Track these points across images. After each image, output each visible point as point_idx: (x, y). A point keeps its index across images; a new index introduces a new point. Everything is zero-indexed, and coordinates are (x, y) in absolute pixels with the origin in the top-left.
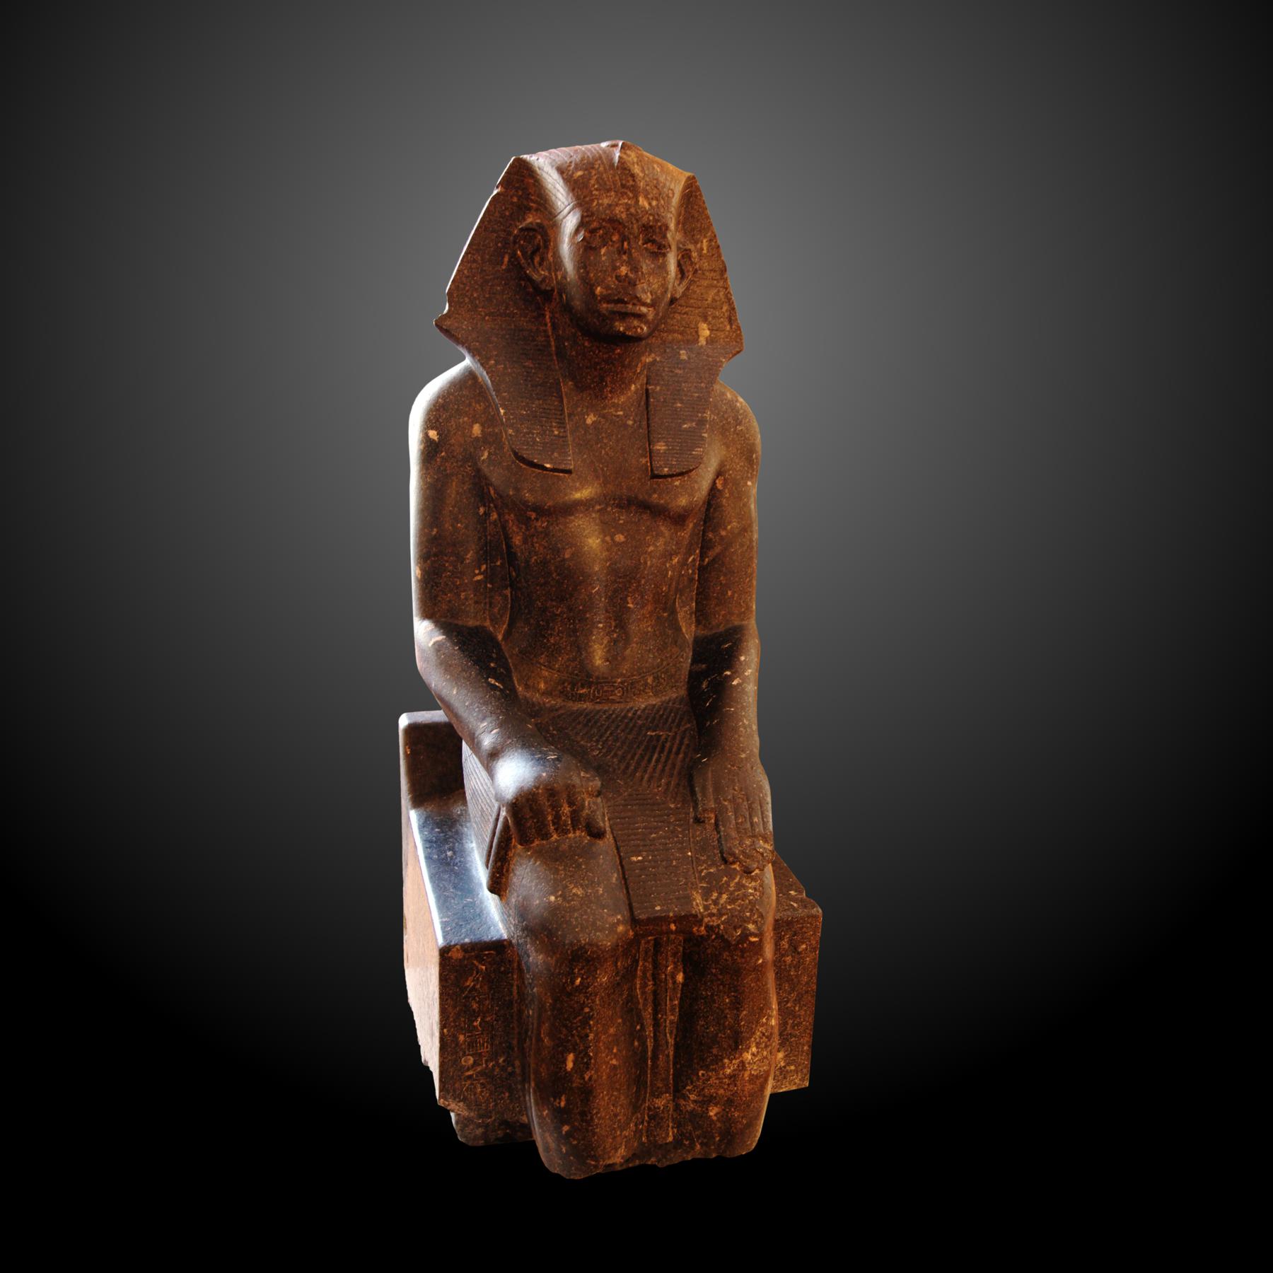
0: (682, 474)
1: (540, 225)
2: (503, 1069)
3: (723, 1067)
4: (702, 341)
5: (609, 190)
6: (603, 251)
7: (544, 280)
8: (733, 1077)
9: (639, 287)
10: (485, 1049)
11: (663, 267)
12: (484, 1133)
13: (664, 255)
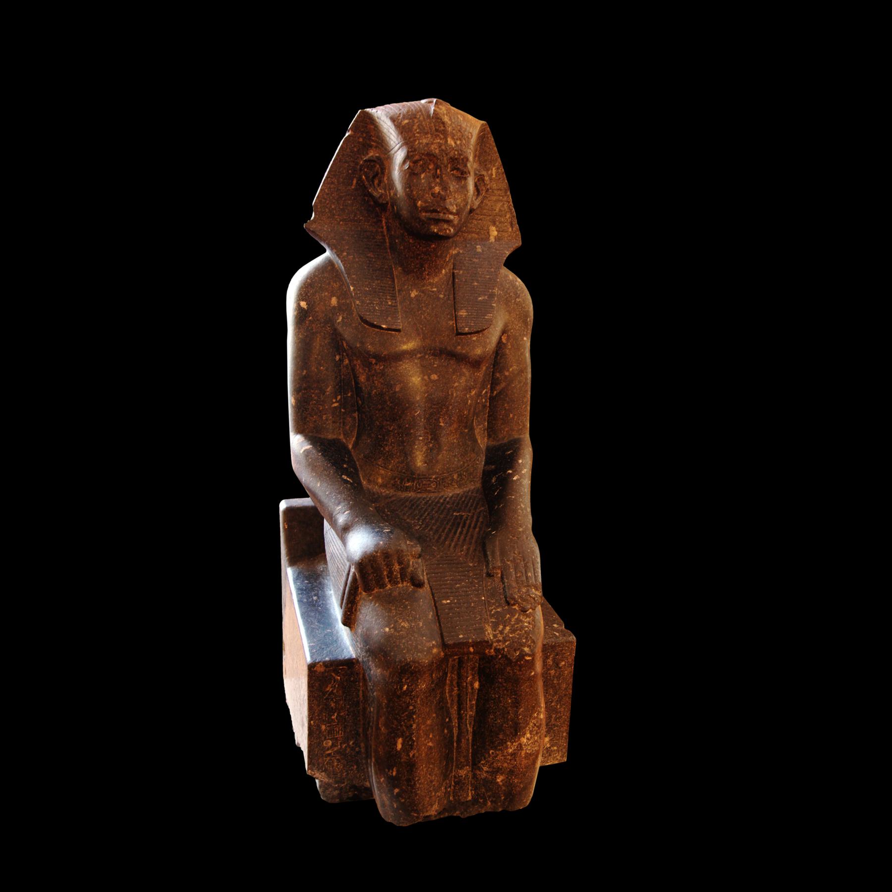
0: (478, 332)
1: (378, 158)
2: (353, 749)
3: (507, 748)
4: (492, 239)
5: (427, 133)
6: (423, 176)
7: (381, 196)
8: (513, 755)
9: (448, 201)
10: (340, 735)
11: (465, 187)
12: (339, 794)
13: (465, 179)
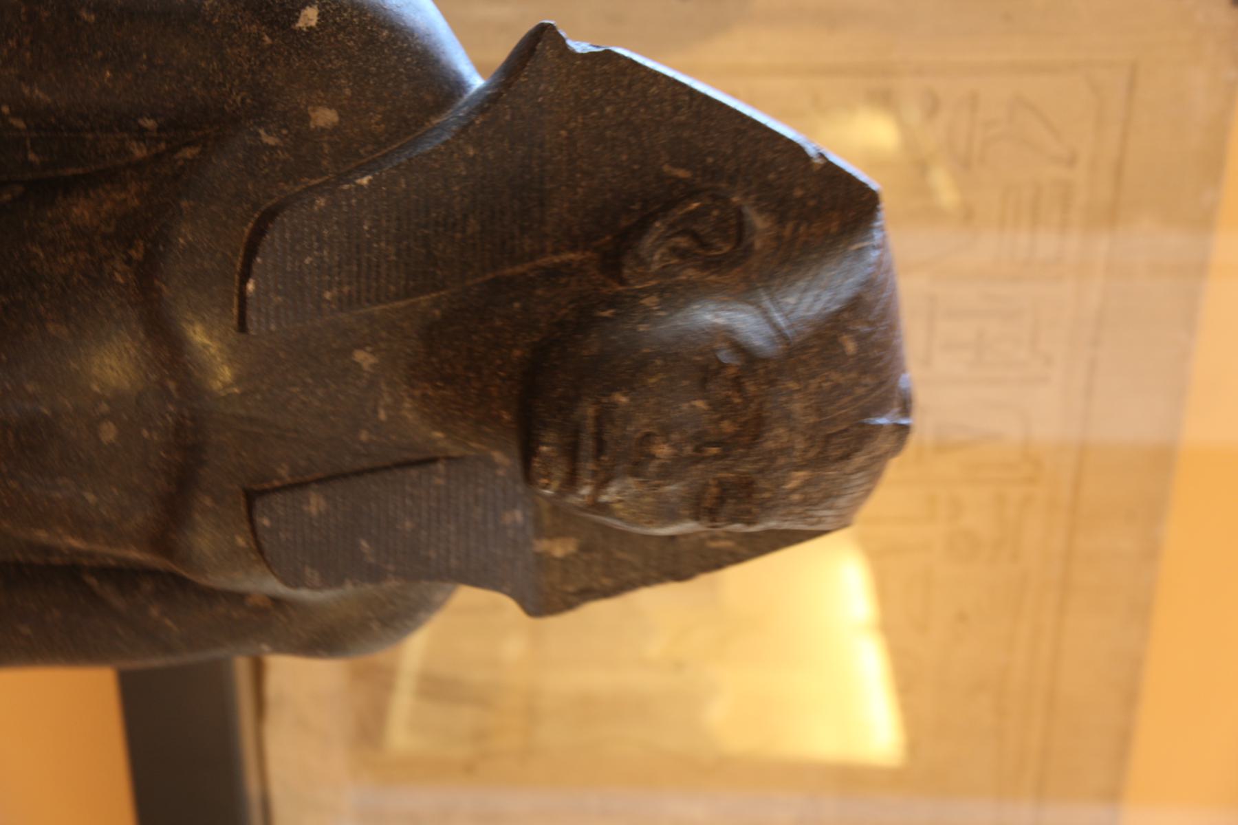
1: (749, 250)
4: (543, 545)
5: (819, 411)
6: (700, 404)
7: (642, 262)
9: (631, 481)
11: (673, 517)
13: (696, 517)
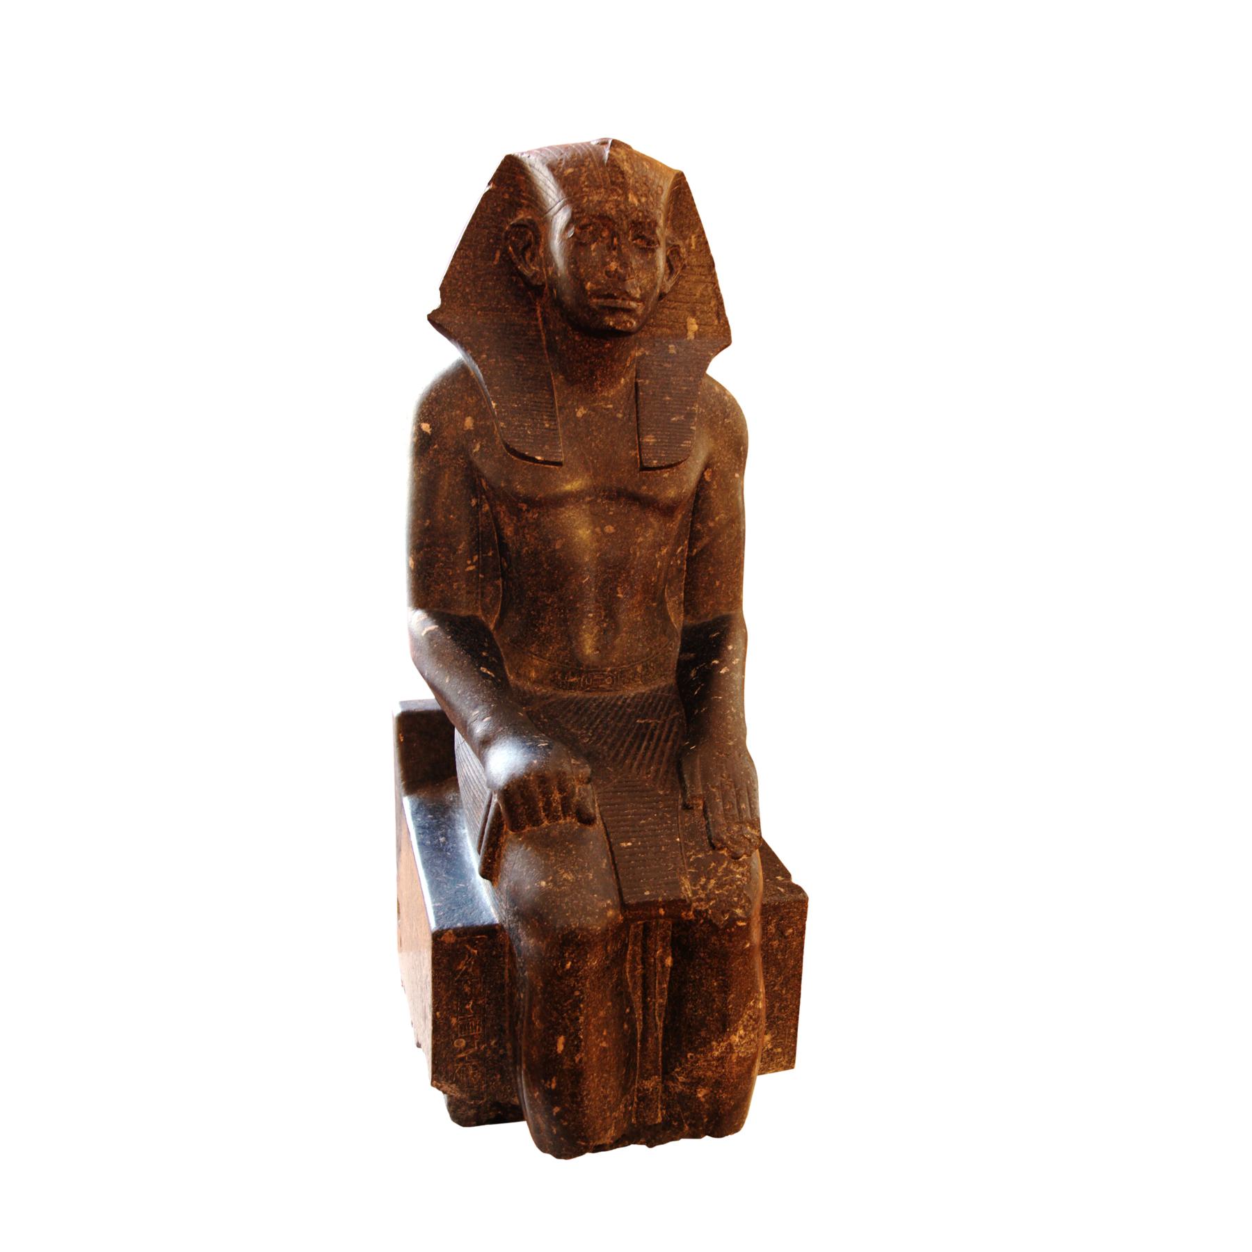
0: (670, 466)
1: (531, 222)
2: (495, 1051)
3: (711, 1050)
4: (691, 336)
5: (599, 187)
6: (593, 247)
7: (535, 275)
8: (721, 1059)
9: (629, 282)
10: (477, 1032)
11: (652, 263)
13: (653, 251)
